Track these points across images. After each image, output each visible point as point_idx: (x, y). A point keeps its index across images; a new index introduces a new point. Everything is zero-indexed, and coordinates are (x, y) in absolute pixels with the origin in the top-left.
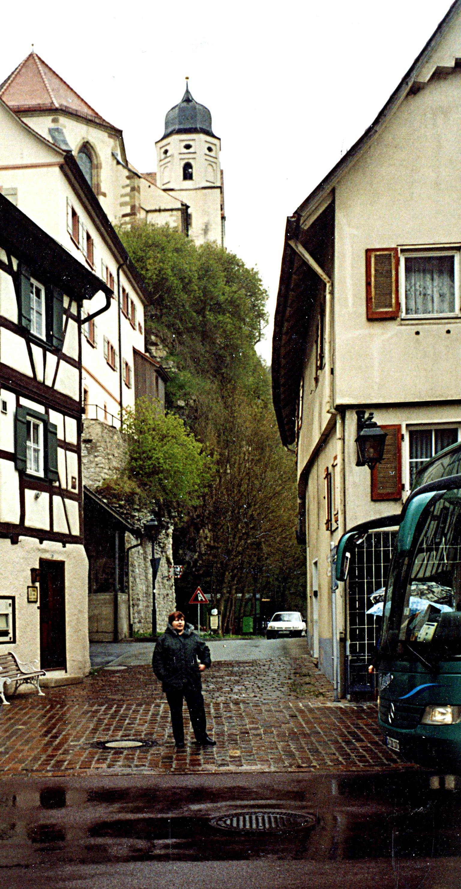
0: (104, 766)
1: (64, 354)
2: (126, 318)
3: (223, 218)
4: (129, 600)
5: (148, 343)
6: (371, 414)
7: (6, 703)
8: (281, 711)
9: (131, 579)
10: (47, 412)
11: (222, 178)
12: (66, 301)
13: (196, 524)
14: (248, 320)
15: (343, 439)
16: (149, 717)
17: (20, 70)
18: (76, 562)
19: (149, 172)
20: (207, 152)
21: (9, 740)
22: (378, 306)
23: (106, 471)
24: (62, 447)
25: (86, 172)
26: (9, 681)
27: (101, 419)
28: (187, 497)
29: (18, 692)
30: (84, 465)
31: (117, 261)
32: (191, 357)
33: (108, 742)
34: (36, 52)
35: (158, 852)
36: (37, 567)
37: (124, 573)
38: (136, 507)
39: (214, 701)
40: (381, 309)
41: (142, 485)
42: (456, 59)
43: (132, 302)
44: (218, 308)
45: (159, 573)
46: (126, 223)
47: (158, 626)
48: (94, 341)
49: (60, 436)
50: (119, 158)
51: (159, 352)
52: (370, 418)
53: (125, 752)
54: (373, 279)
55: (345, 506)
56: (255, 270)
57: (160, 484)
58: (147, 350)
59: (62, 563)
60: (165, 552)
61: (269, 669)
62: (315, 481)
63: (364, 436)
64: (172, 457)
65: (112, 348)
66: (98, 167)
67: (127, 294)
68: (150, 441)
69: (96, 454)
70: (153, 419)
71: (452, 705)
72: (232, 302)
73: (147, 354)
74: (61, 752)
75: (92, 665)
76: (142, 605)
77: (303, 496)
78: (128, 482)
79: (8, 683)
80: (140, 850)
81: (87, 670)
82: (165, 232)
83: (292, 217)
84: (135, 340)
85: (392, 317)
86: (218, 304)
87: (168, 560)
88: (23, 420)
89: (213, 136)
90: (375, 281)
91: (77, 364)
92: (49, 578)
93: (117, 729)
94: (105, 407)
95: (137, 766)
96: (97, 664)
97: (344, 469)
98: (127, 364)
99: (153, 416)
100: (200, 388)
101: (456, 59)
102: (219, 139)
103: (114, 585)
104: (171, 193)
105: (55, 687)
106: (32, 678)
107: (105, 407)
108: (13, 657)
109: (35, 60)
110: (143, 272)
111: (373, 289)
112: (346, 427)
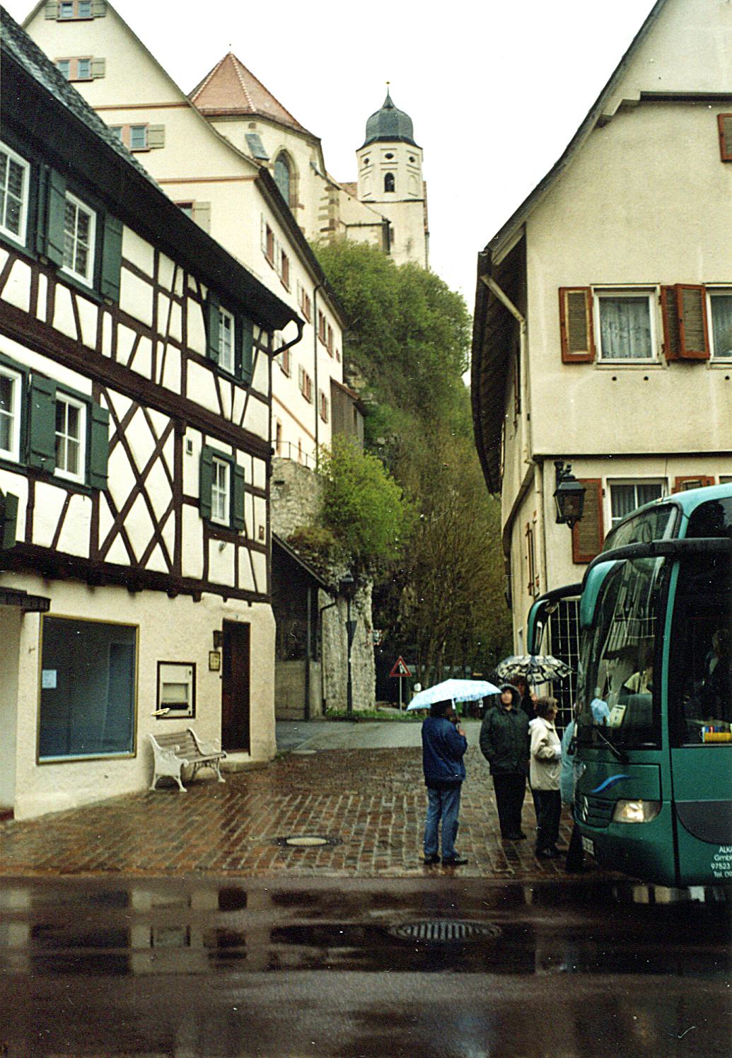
0: (284, 866)
1: (253, 389)
2: (323, 344)
3: (427, 233)
4: (322, 670)
5: (346, 372)
6: (569, 467)
7: (183, 789)
8: (480, 808)
9: (325, 645)
10: (234, 453)
11: (425, 190)
12: (256, 332)
13: (399, 580)
14: (453, 348)
15: (542, 493)
16: (336, 810)
17: (217, 71)
18: (262, 622)
19: (349, 181)
20: (409, 162)
21: (183, 833)
22: (572, 349)
23: (299, 517)
24: (249, 492)
25: (284, 190)
26: (187, 762)
27: (295, 458)
28: (387, 550)
29: (196, 777)
30: (276, 509)
31: (314, 282)
32: (392, 389)
33: (290, 838)
34: (232, 53)
35: (331, 960)
36: (220, 629)
37: (317, 638)
38: (331, 560)
39: (408, 793)
40: (576, 354)
41: (338, 535)
42: (642, 92)
43: (329, 328)
44: (420, 335)
45: (355, 640)
46: (323, 239)
47: (354, 703)
48: (288, 370)
49: (248, 480)
50: (318, 168)
51: (359, 383)
52: (568, 471)
53: (307, 850)
54: (567, 319)
55: (546, 568)
56: (459, 294)
57: (358, 534)
58: (345, 380)
59: (247, 626)
60: (364, 614)
61: (472, 758)
62: (518, 537)
63: (560, 491)
64: (367, 503)
65: (307, 377)
66: (296, 177)
67: (324, 318)
68: (347, 484)
69: (288, 498)
70: (351, 458)
71: (644, 800)
72: (433, 329)
73: (345, 385)
74: (238, 848)
75: (278, 747)
76: (337, 677)
77: (508, 554)
78: (323, 531)
79: (185, 766)
80: (313, 959)
81: (273, 754)
82: (364, 251)
83: (483, 252)
84: (332, 369)
85: (587, 361)
86: (420, 332)
87: (366, 623)
88: (208, 461)
89: (415, 145)
90: (570, 322)
91: (267, 400)
92: (233, 639)
93: (299, 824)
94: (300, 444)
95: (318, 866)
96: (285, 747)
97: (543, 527)
98: (323, 396)
99: (350, 456)
100: (402, 425)
101: (642, 92)
102: (421, 149)
103: (305, 650)
104: (368, 205)
105: (238, 772)
106: (212, 761)
107: (300, 444)
108: (192, 734)
109: (232, 61)
110: (342, 294)
111: (567, 331)
112: (545, 480)
